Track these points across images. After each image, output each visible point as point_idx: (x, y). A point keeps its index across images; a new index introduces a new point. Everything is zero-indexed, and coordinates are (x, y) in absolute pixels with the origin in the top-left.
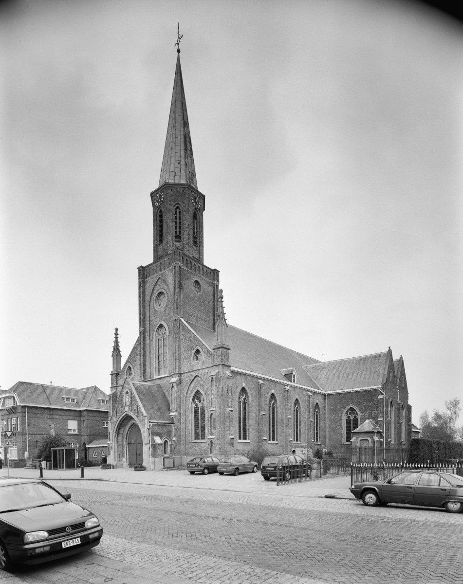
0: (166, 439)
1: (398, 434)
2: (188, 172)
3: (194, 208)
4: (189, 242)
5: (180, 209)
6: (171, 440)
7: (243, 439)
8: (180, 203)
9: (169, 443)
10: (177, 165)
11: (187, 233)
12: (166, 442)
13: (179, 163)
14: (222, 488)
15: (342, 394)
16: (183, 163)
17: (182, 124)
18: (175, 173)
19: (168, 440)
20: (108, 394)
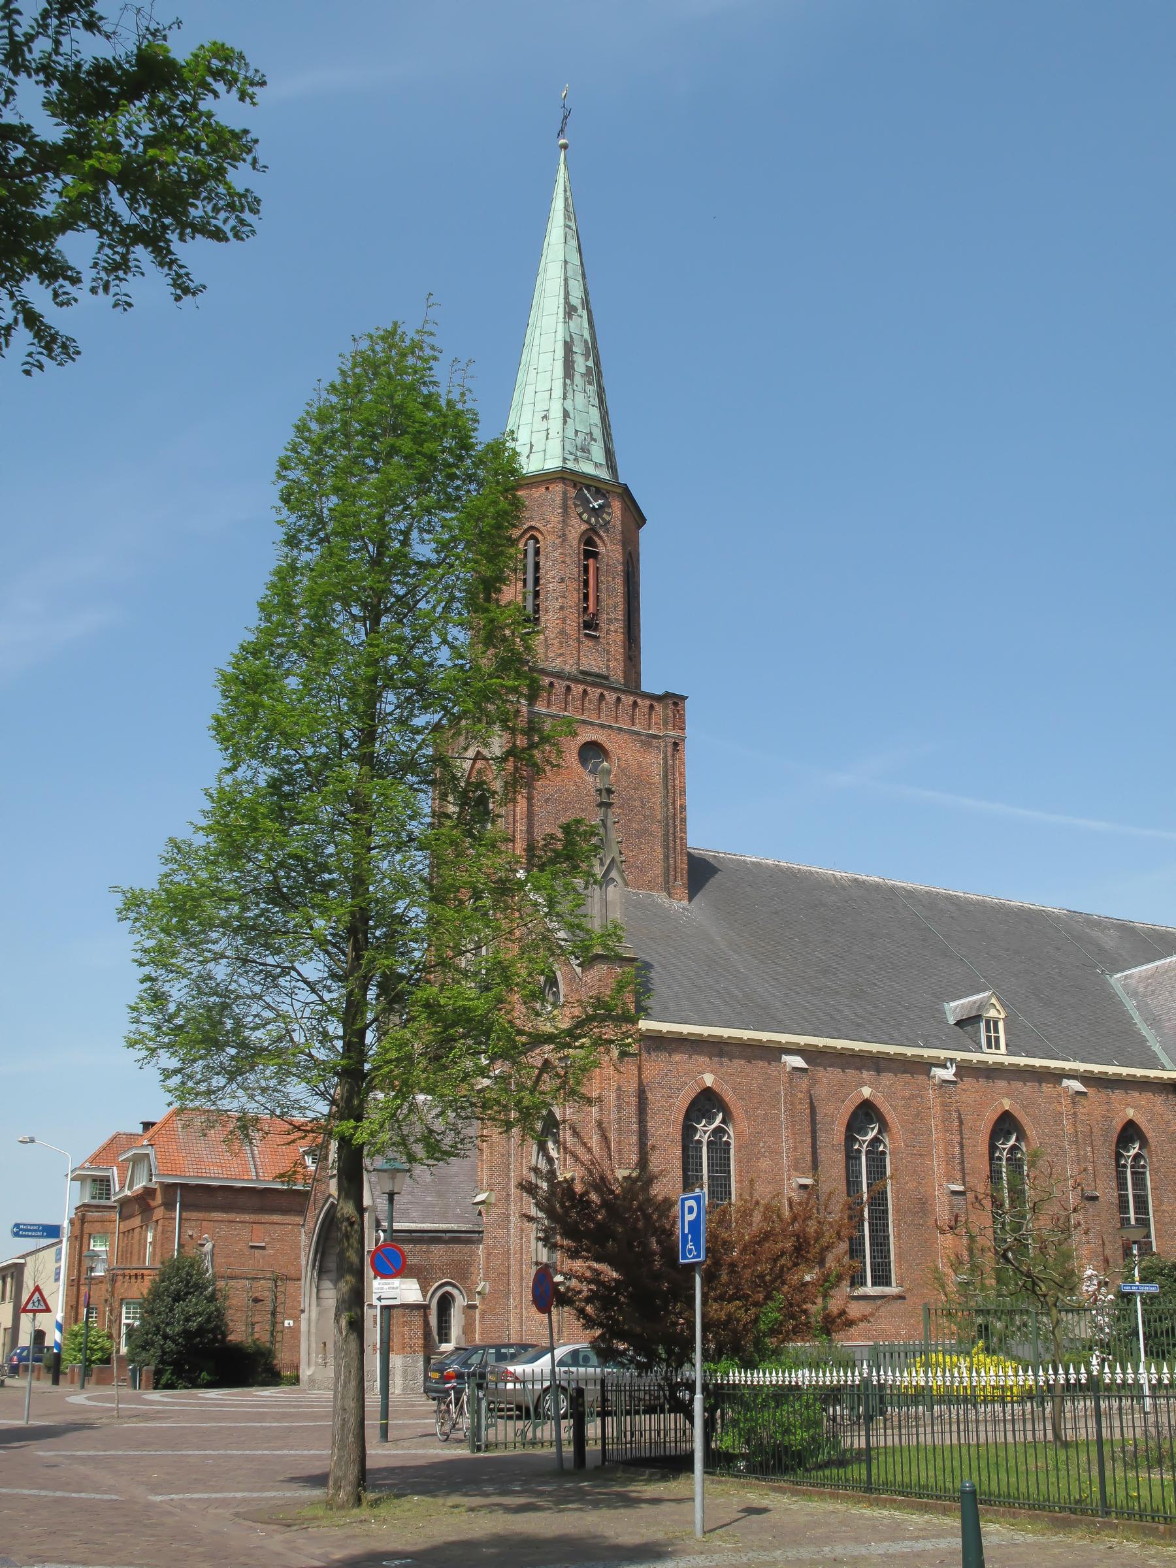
0: (449, 1289)
1: (630, 648)
2: (571, 434)
3: (584, 527)
4: (562, 632)
5: (537, 541)
6: (470, 1293)
7: (874, 1284)
8: (538, 525)
9: (460, 1301)
10: (541, 425)
11: (557, 605)
12: (445, 1303)
13: (545, 417)
14: (665, 1507)
15: (741, 1171)
16: (556, 413)
17: (561, 315)
18: (532, 446)
19: (455, 1292)
20: (159, 1107)
